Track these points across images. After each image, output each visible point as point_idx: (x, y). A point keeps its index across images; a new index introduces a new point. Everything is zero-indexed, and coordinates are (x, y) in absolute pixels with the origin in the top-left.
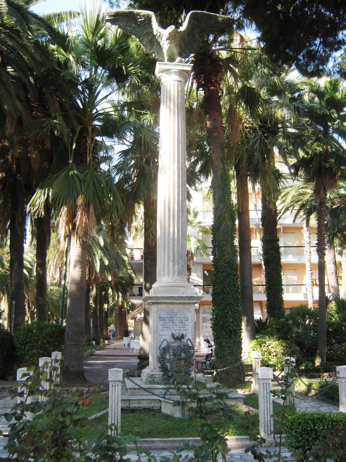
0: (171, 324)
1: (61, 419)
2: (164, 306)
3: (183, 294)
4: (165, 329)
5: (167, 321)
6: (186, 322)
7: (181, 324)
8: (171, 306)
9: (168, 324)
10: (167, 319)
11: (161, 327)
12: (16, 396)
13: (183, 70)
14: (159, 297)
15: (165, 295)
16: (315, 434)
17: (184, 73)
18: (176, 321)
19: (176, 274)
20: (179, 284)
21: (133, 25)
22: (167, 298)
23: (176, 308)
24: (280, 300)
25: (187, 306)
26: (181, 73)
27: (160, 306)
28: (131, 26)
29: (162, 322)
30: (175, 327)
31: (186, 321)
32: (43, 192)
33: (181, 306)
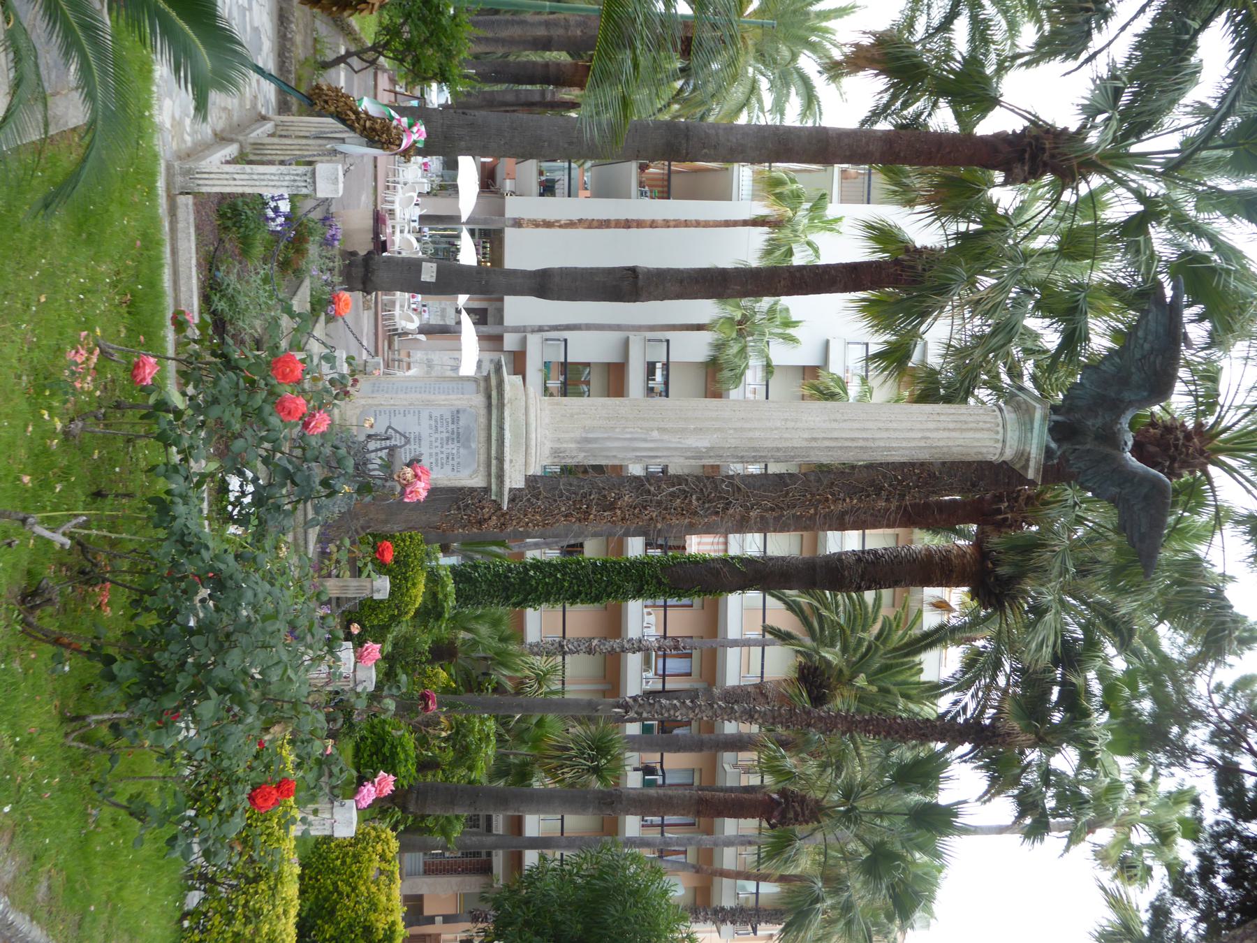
0: (445, 435)
1: (1133, 370)
2: (483, 420)
3: (511, 461)
4: (433, 423)
5: (451, 426)
6: (448, 468)
7: (444, 456)
8: (482, 436)
9: (444, 429)
10: (454, 426)
11: (436, 414)
12: (94, 111)
13: (1028, 460)
14: (502, 413)
15: (507, 426)
16: (700, 706)
17: (1023, 462)
18: (451, 446)
19: (557, 445)
20: (533, 451)
21: (1147, 346)
22: (501, 428)
23: (478, 444)
24: (918, 651)
25: (482, 469)
26: (1022, 454)
27: (483, 412)
28: (1145, 339)
29: (448, 416)
30: (438, 444)
31: (450, 468)
32: (137, 39)
33: (483, 458)
